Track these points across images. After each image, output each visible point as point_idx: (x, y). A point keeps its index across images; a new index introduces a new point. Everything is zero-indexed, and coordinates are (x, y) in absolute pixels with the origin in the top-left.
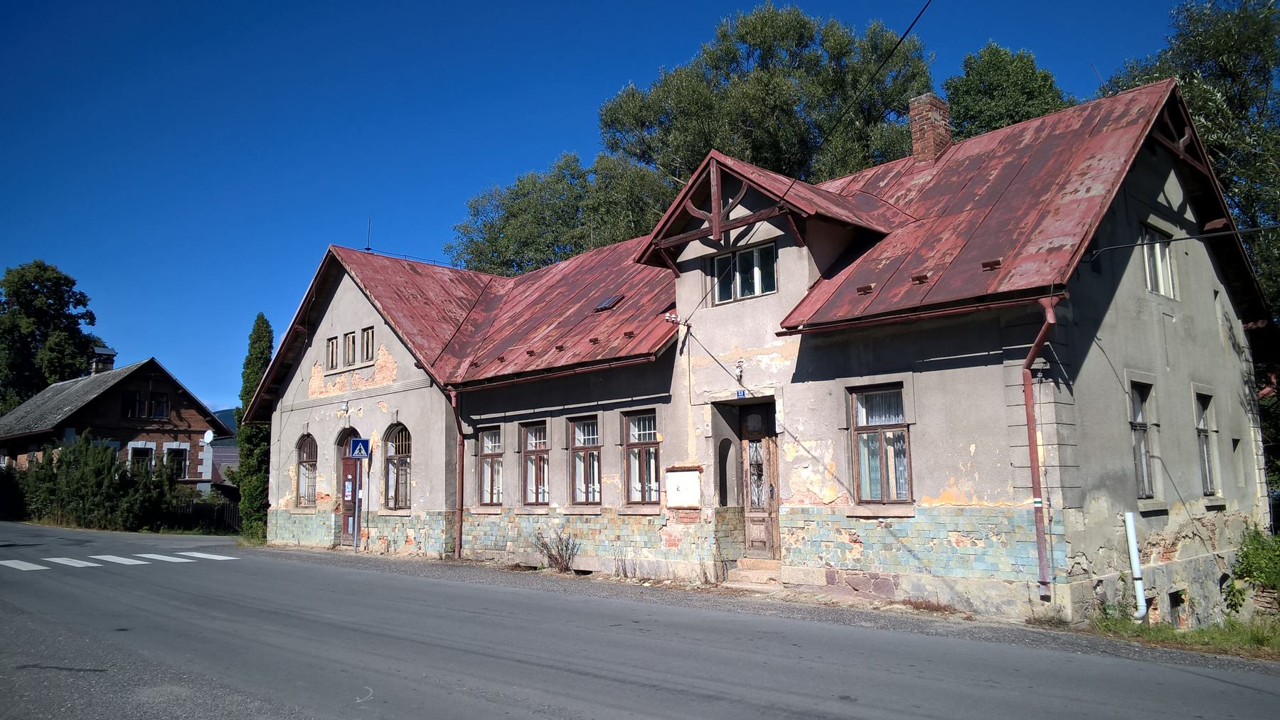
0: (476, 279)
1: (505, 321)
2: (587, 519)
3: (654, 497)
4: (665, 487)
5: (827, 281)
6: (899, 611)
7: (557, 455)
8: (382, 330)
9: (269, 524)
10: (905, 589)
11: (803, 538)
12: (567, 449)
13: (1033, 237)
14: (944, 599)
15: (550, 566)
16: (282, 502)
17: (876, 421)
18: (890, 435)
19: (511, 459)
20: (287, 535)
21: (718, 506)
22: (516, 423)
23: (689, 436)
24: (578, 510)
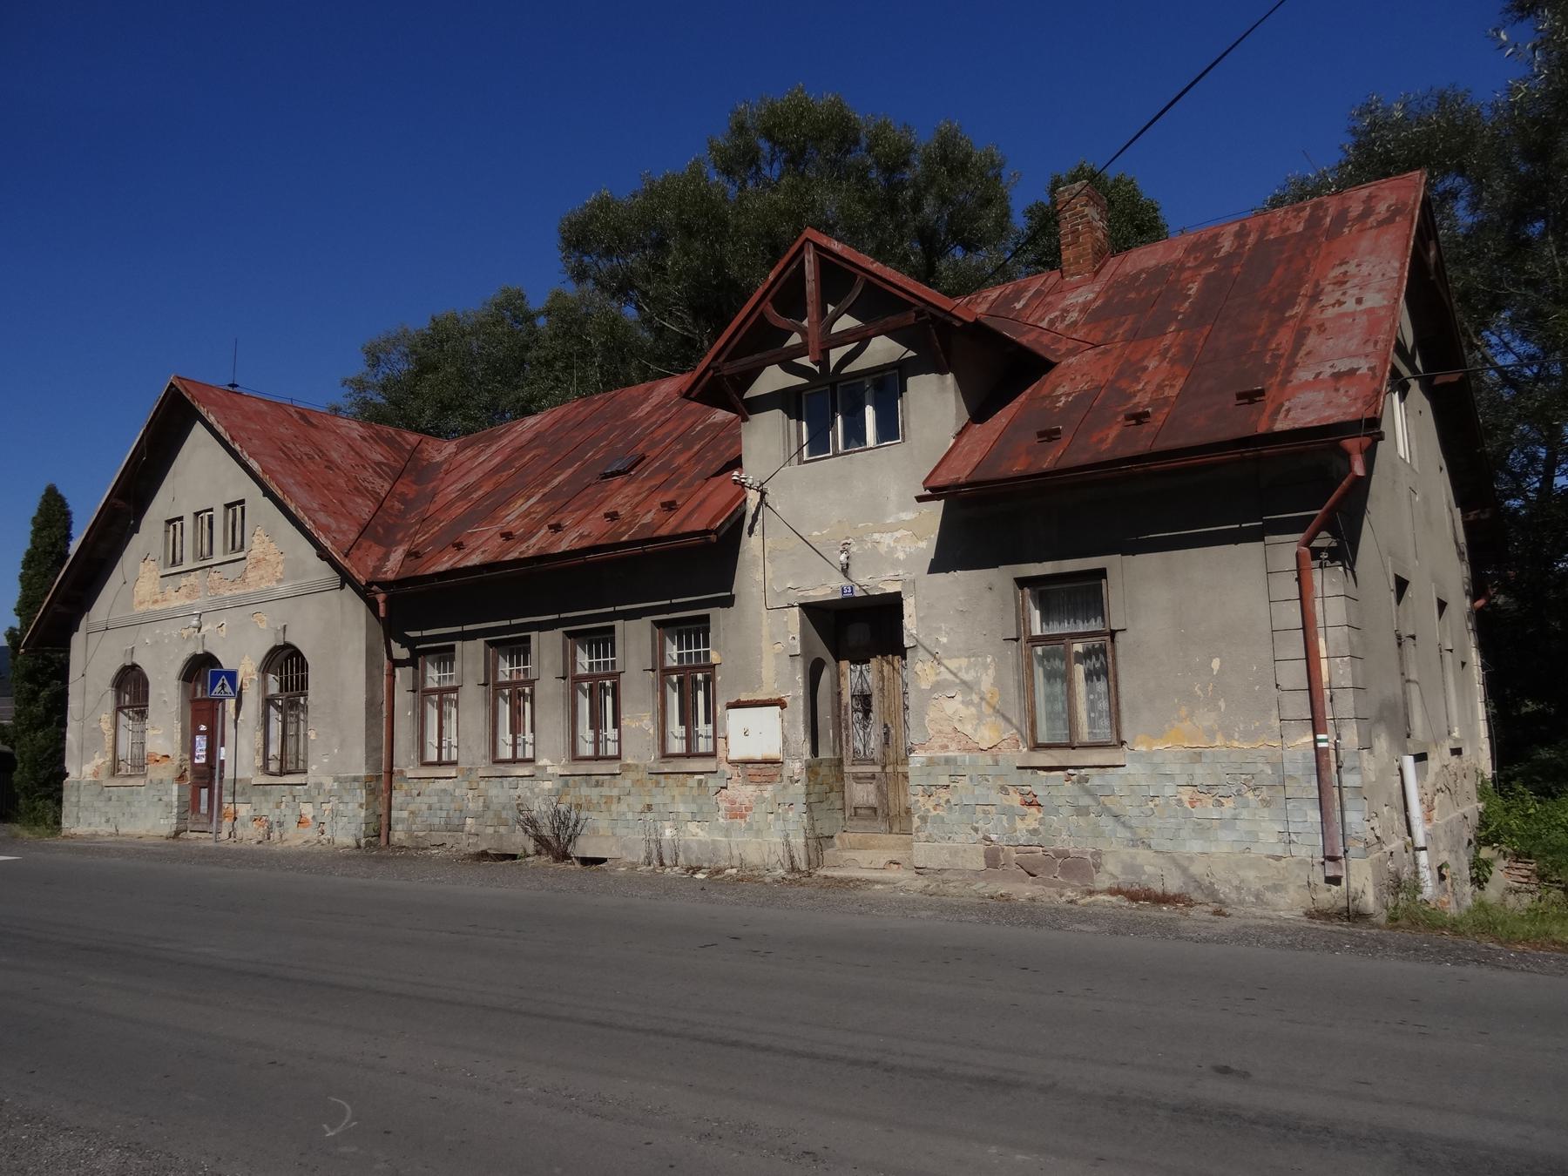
0: (399, 439)
1: (453, 496)
2: (597, 782)
3: (703, 746)
4: (724, 729)
5: (978, 425)
6: (1107, 904)
7: (549, 687)
8: (260, 505)
9: (65, 804)
10: (1112, 871)
11: (948, 801)
12: (564, 678)
13: (1298, 359)
14: (1173, 885)
15: (538, 853)
16: (88, 769)
17: (1056, 629)
18: (1078, 647)
19: (472, 696)
20: (97, 819)
21: (809, 757)
22: (481, 642)
23: (764, 655)
24: (583, 768)
